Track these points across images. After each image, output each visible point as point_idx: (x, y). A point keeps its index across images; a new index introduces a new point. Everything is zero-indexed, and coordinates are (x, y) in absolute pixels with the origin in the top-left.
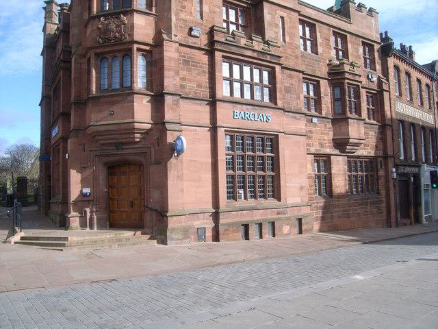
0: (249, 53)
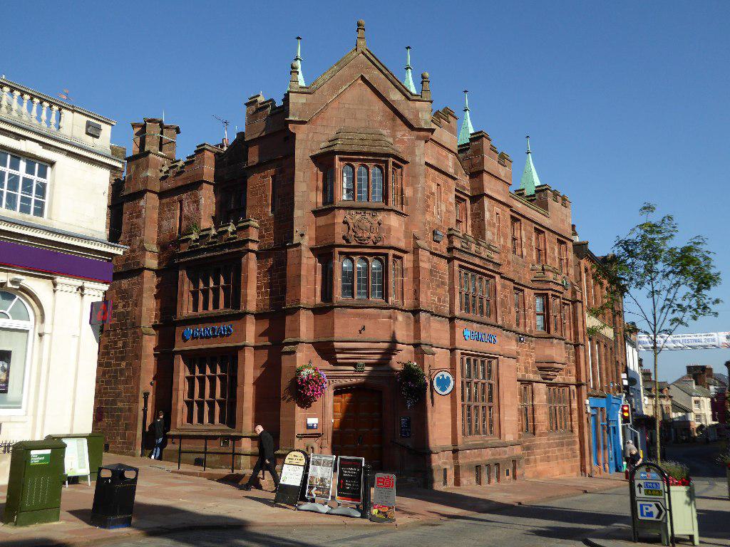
0: (477, 261)
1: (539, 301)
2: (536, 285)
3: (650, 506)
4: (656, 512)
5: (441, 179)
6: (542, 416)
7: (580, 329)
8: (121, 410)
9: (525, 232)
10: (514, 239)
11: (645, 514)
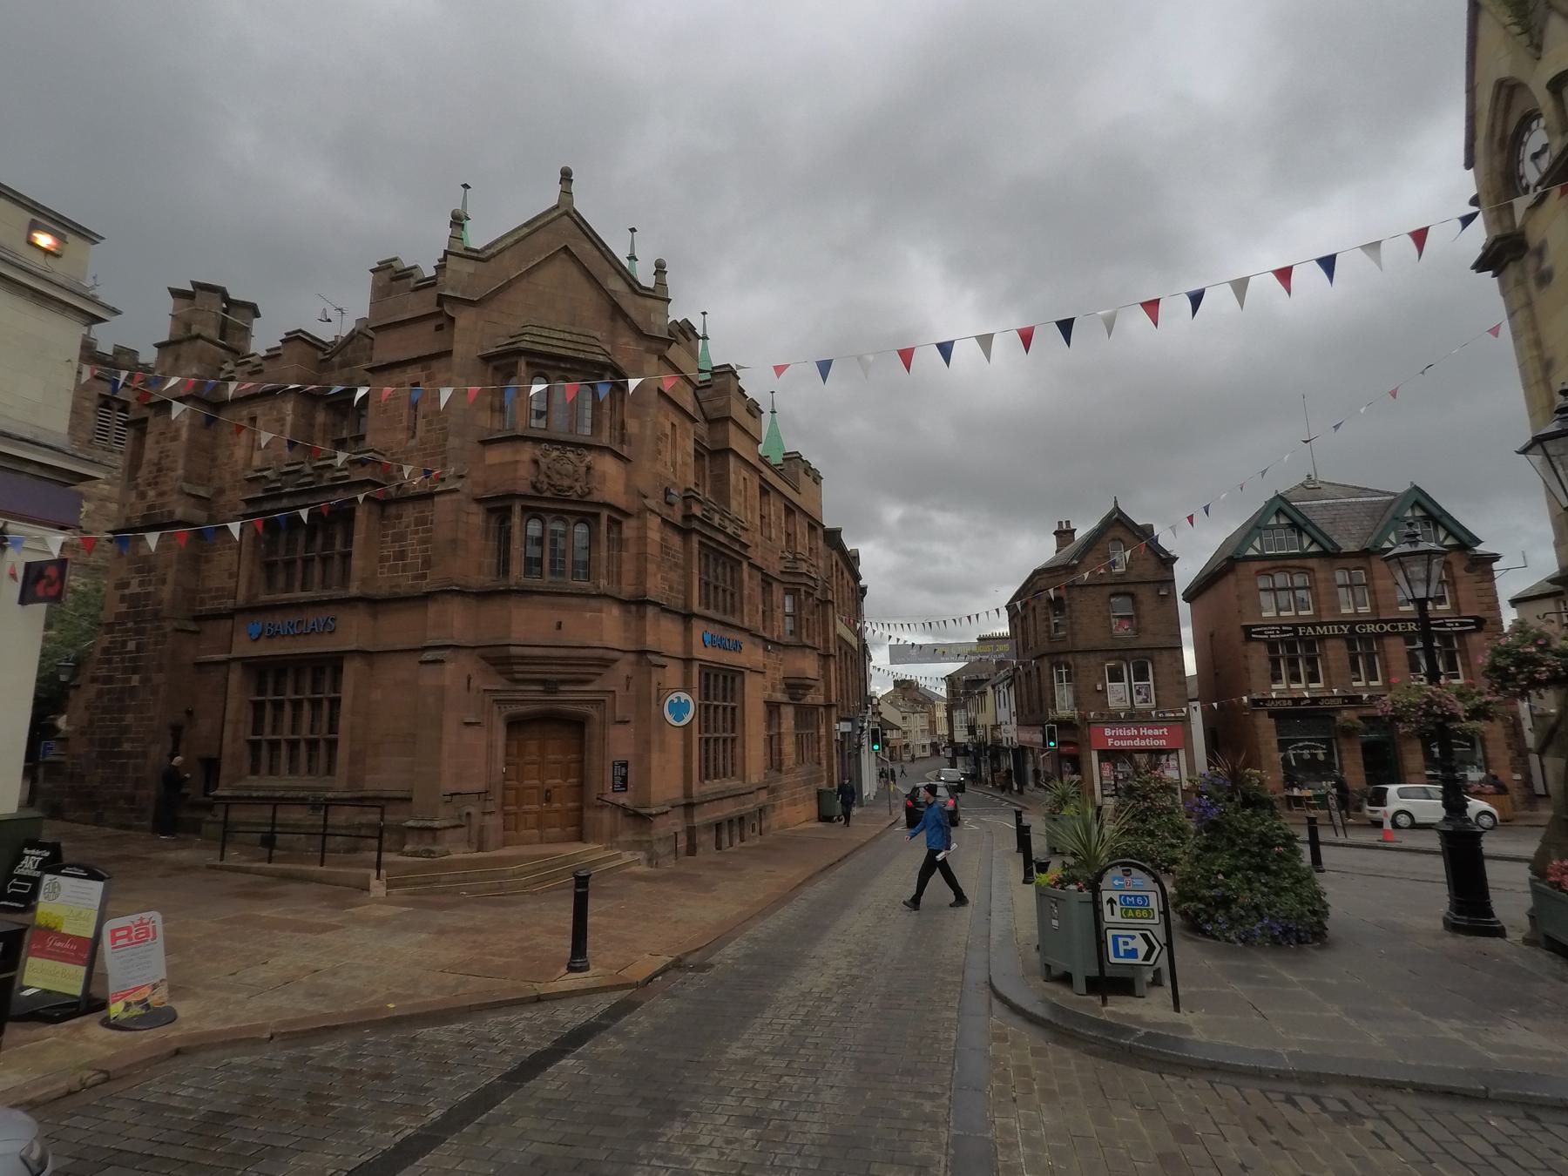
1: (788, 601)
2: (786, 578)
3: (1133, 937)
4: (1143, 949)
5: (676, 418)
6: (789, 746)
7: (831, 635)
8: (129, 755)
9: (775, 508)
10: (762, 517)
11: (1122, 954)
